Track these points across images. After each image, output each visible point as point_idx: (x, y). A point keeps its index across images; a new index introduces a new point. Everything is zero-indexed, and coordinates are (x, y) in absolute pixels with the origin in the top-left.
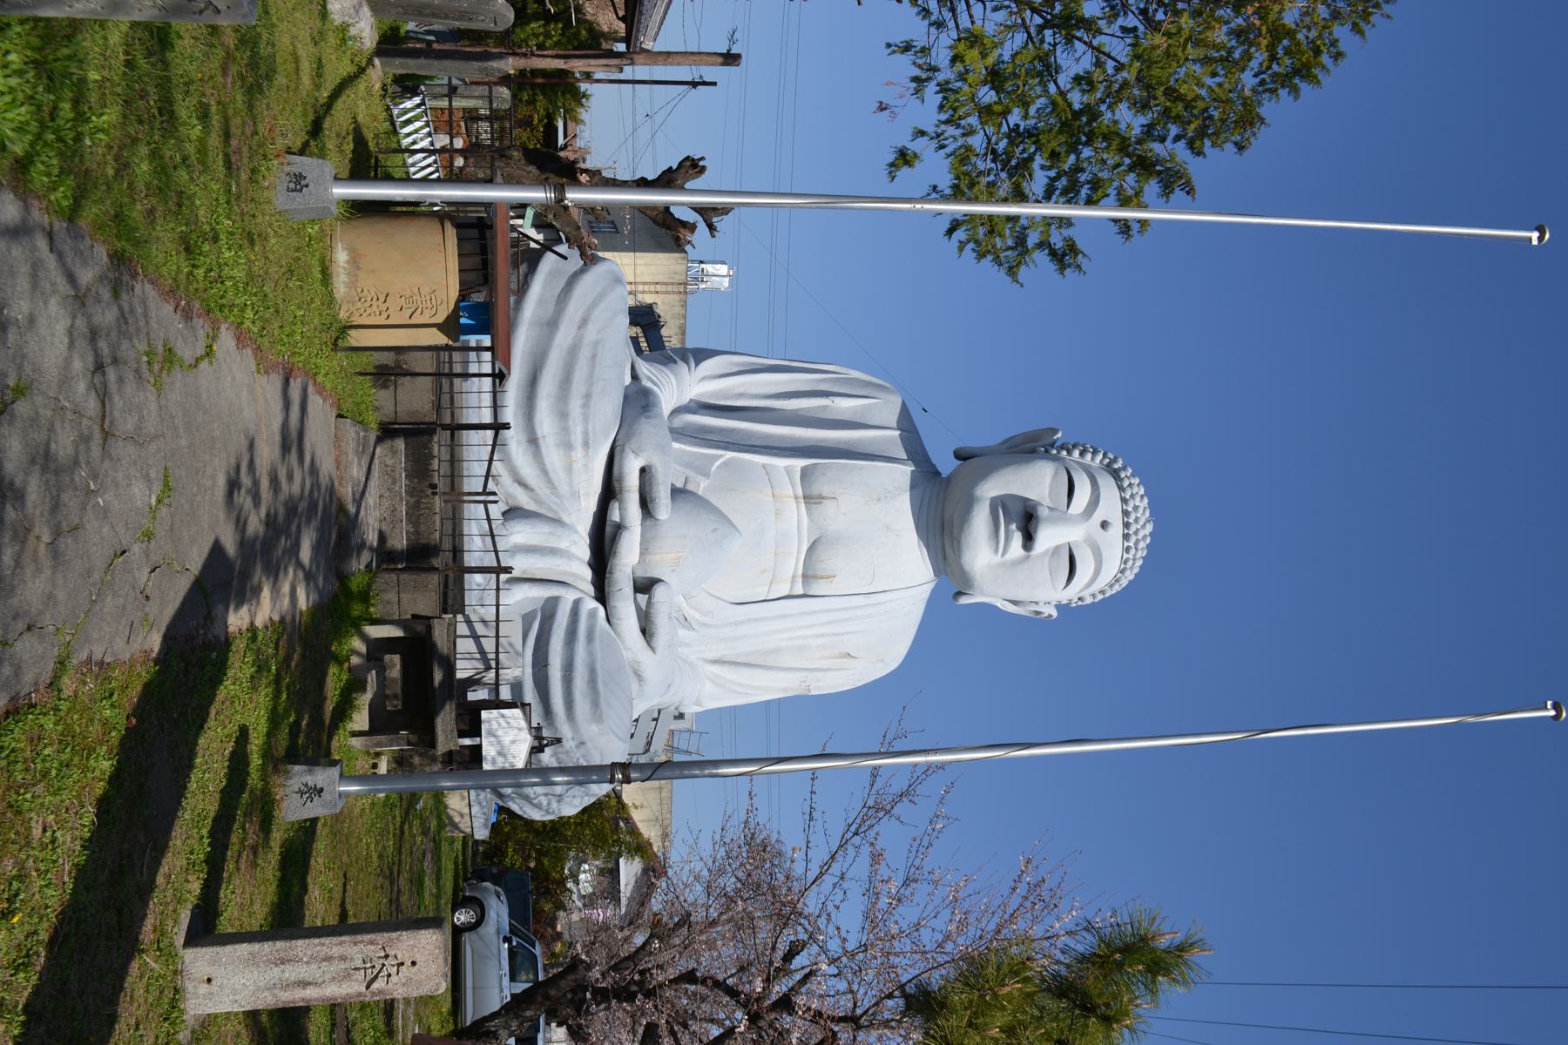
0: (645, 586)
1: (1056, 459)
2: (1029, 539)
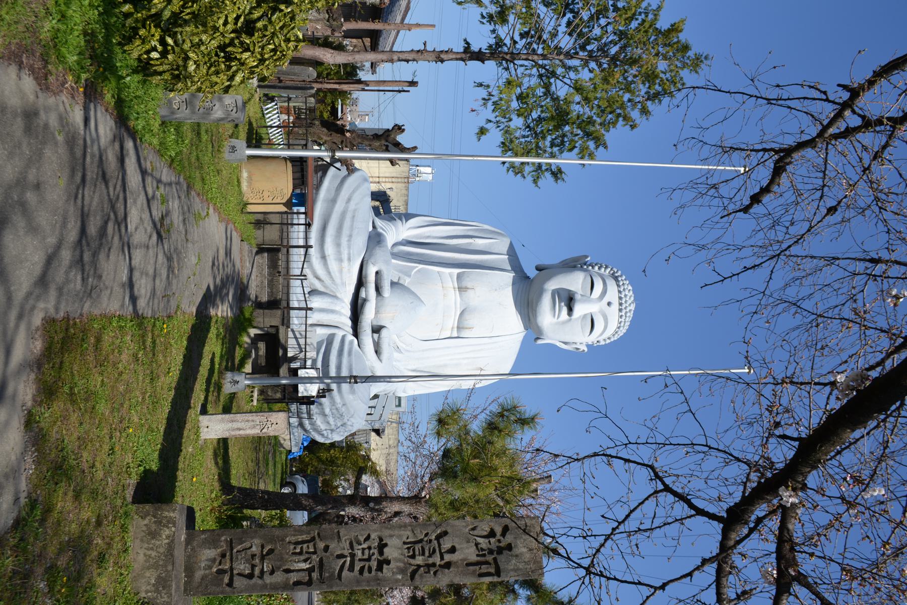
0: (377, 330)
1: (586, 270)
2: (570, 310)
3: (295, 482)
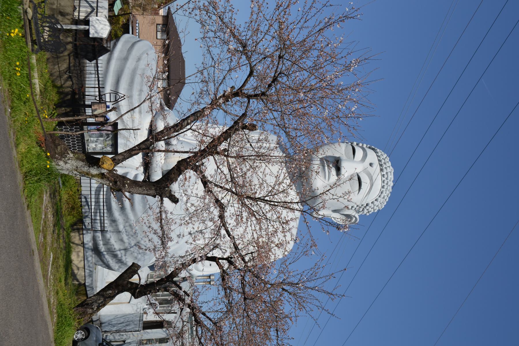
2: (338, 170)
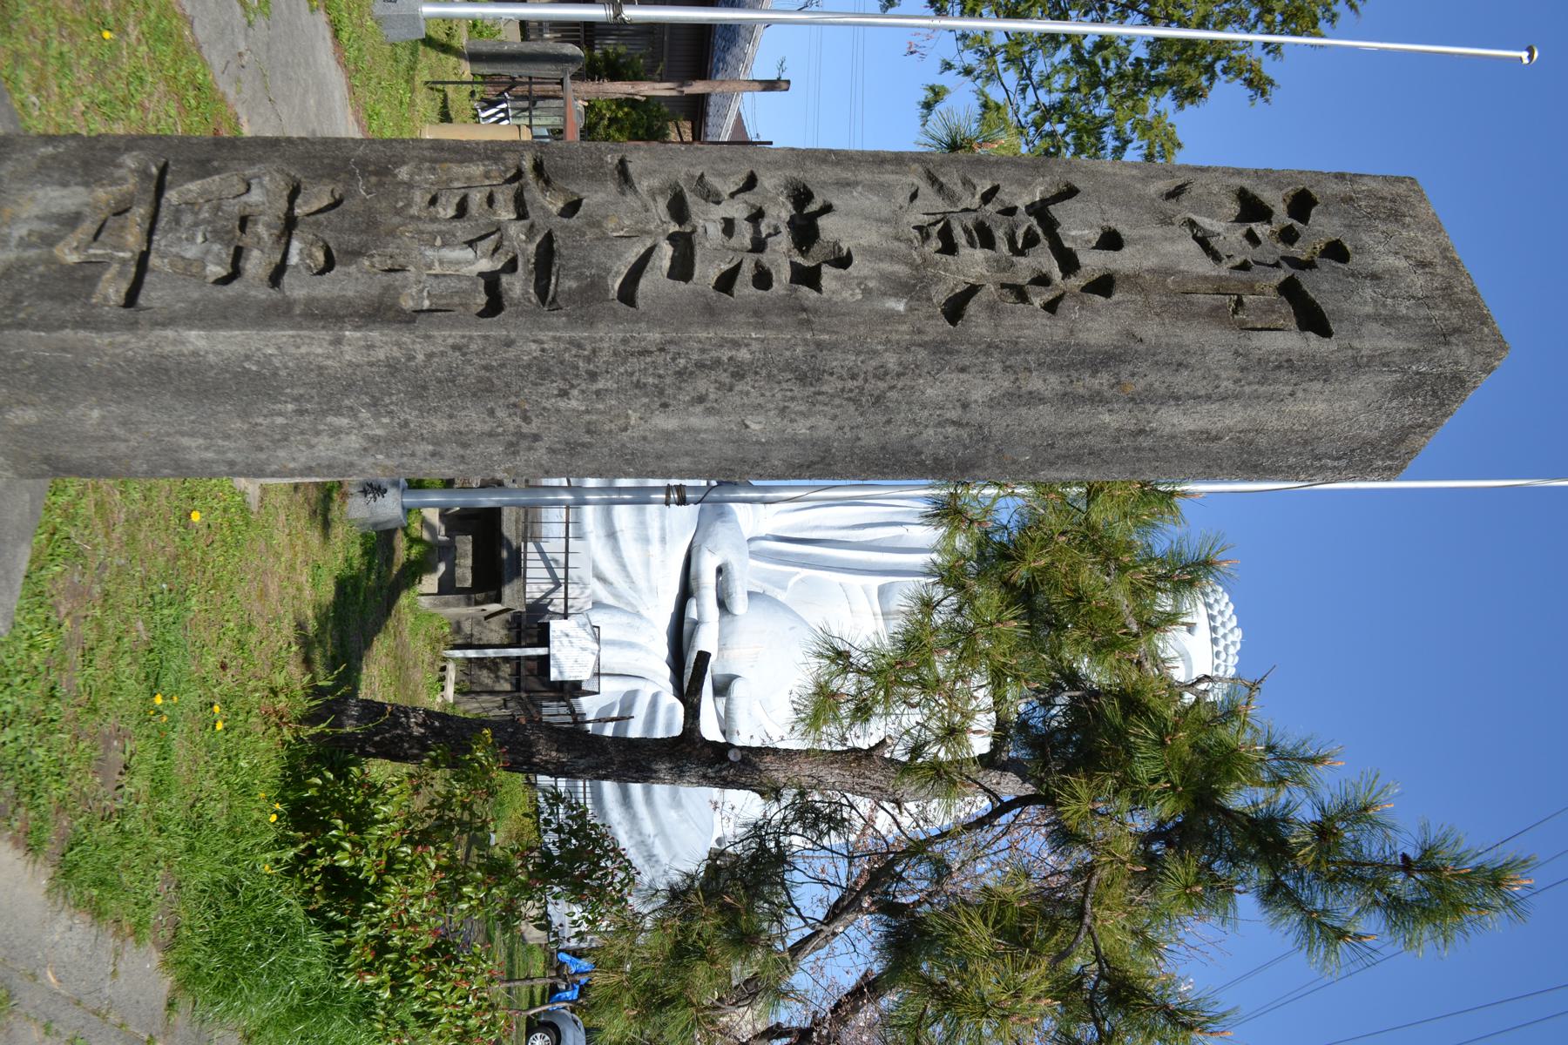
3: (557, 1021)
